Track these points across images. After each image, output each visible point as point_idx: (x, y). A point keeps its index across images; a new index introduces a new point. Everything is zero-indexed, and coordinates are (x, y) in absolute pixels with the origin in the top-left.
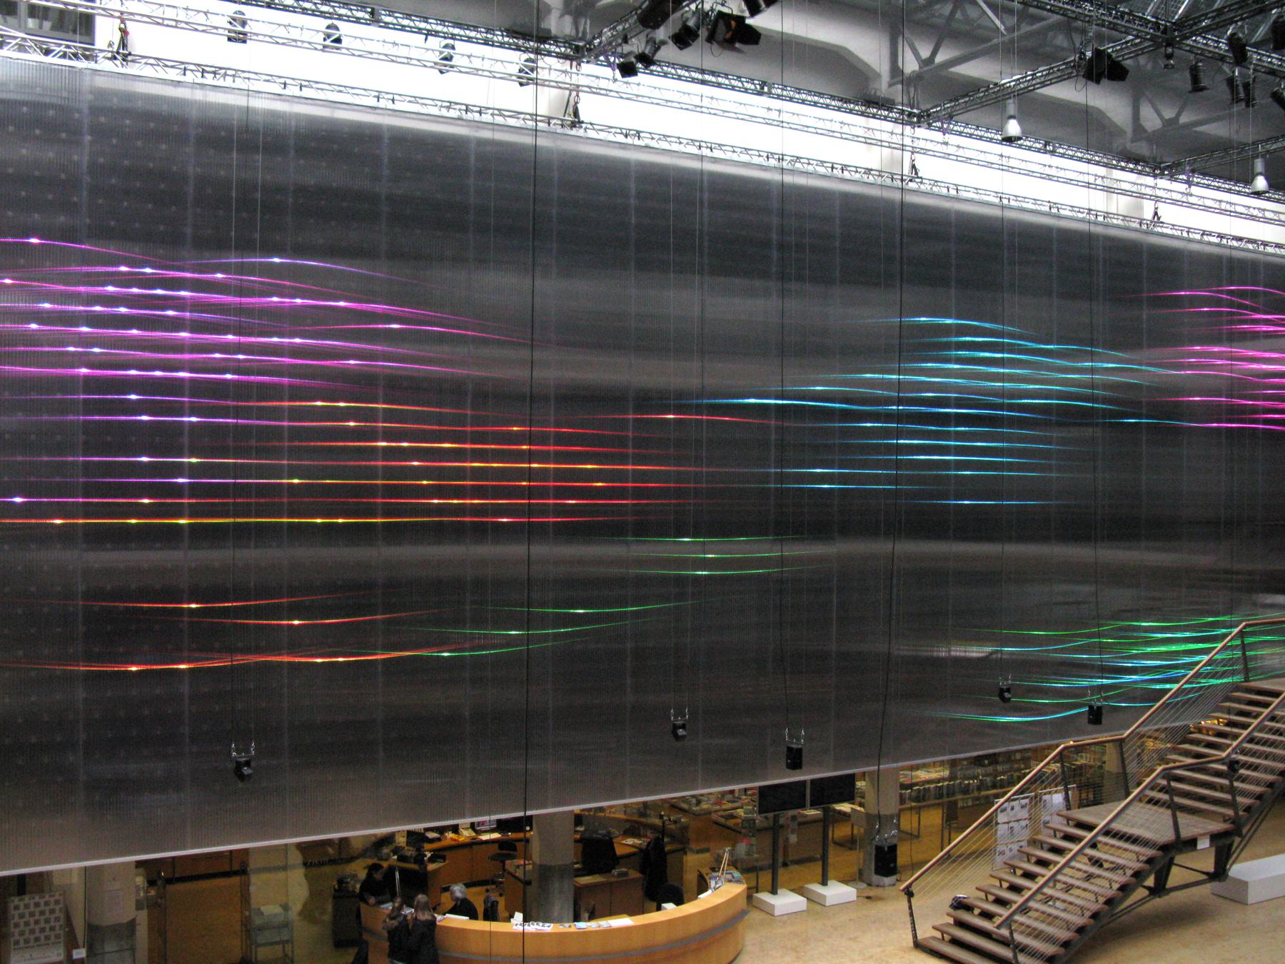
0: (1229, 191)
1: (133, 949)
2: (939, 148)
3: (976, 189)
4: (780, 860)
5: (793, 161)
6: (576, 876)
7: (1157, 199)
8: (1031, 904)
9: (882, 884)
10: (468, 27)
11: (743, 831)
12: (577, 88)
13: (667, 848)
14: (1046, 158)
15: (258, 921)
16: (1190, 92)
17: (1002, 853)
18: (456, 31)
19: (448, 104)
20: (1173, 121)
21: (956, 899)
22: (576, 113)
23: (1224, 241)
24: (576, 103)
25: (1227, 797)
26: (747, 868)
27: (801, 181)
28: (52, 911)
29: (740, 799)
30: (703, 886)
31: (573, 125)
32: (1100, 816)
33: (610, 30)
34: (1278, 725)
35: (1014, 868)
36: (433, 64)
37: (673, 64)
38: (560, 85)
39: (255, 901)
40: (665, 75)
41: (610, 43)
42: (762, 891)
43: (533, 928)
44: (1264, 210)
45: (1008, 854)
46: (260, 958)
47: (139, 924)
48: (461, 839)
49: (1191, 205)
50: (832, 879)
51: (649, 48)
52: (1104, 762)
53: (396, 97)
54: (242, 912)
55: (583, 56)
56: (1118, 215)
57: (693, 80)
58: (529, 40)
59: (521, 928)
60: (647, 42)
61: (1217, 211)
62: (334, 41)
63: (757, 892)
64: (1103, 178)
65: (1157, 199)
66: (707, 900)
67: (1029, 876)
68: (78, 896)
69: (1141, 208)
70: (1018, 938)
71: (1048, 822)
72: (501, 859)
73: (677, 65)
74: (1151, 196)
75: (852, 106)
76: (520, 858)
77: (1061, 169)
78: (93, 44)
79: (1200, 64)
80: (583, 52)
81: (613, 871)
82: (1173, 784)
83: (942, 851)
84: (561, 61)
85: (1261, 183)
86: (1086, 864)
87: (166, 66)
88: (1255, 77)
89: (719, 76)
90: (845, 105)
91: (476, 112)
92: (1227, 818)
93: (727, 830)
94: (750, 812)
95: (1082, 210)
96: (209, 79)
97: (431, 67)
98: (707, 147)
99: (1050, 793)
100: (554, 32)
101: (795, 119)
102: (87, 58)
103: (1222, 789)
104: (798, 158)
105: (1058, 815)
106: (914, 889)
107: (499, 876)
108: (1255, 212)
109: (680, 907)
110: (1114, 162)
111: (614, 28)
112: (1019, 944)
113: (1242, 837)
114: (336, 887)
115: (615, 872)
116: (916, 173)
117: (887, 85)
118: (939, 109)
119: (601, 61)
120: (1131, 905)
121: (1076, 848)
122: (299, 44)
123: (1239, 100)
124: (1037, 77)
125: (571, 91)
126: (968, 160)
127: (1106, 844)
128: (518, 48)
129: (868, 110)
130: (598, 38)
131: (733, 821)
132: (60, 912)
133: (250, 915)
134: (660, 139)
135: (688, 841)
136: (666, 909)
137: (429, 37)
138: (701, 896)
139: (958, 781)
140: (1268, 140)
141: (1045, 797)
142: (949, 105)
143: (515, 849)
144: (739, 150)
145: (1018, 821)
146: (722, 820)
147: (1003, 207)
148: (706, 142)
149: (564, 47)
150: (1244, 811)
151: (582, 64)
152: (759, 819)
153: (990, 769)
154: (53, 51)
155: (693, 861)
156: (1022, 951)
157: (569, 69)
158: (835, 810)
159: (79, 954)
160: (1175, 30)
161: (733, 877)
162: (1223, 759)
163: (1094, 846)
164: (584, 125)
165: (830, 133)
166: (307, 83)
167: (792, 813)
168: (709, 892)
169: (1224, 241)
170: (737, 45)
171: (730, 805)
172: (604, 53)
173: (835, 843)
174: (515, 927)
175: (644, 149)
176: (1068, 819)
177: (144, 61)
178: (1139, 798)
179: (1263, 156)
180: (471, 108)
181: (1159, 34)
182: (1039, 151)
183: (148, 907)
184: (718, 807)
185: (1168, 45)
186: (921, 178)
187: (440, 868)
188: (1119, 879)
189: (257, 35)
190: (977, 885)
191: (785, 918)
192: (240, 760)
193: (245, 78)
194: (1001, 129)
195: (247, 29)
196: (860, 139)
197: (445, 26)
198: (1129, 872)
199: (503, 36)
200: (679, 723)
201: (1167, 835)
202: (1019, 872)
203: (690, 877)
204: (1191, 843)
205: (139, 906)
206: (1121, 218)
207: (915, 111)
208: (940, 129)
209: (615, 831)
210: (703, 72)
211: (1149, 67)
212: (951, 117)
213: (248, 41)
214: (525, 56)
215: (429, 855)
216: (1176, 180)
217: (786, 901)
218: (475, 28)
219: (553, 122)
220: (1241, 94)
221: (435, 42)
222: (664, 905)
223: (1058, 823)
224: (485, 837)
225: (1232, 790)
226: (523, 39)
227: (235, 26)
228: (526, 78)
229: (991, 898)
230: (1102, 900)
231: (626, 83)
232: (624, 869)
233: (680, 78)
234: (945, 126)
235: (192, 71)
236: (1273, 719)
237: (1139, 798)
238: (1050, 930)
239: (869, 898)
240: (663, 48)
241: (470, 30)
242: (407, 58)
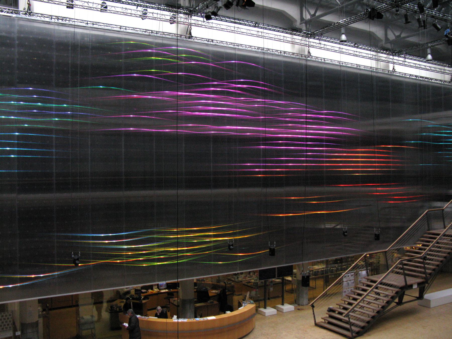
0: (419, 61)
1: (37, 332)
2: (318, 45)
3: (331, 60)
4: (267, 298)
5: (266, 50)
6: (195, 304)
7: (394, 63)
8: (355, 309)
9: (303, 304)
10: (152, 3)
11: (254, 287)
12: (191, 24)
13: (227, 293)
14: (355, 49)
15: (82, 321)
16: (405, 23)
17: (345, 292)
18: (148, 5)
19: (145, 30)
20: (399, 36)
21: (329, 308)
22: (190, 34)
23: (418, 78)
24: (190, 30)
25: (423, 270)
26: (256, 300)
27: (270, 57)
28: (8, 318)
29: (252, 276)
30: (240, 305)
31: (189, 38)
32: (379, 278)
33: (202, 4)
34: (440, 245)
35: (349, 297)
36: (139, 16)
37: (224, 16)
38: (185, 23)
39: (81, 315)
40: (222, 20)
41: (202, 9)
42: (261, 307)
43: (180, 320)
44: (431, 67)
45: (347, 292)
46: (83, 335)
47: (40, 323)
48: (154, 292)
49: (406, 65)
50: (285, 303)
51: (216, 9)
52: (380, 261)
53: (127, 28)
54: (76, 318)
55: (193, 14)
56: (380, 69)
57: (231, 22)
58: (173, 8)
59: (177, 321)
60: (215, 8)
61: (415, 67)
62: (104, 8)
63: (259, 308)
64: (375, 56)
65: (394, 63)
66: (242, 310)
67: (355, 299)
68: (17, 315)
69: (388, 66)
70: (351, 320)
71: (361, 281)
72: (168, 299)
73: (226, 16)
74: (392, 62)
75: (287, 31)
76: (175, 298)
77: (361, 53)
78: (18, 9)
79: (408, 14)
80: (192, 12)
81: (208, 301)
82: (405, 267)
83: (324, 291)
84: (185, 15)
85: (430, 57)
86: (374, 294)
87: (45, 17)
88: (427, 19)
89: (240, 21)
90: (285, 31)
91: (155, 33)
92: (423, 277)
93: (248, 287)
94: (257, 280)
95: (368, 67)
96: (60, 21)
97: (139, 17)
98: (237, 46)
99: (361, 271)
100: (182, 5)
101: (267, 35)
102: (16, 13)
103: (420, 267)
104: (268, 49)
105: (364, 278)
106: (315, 305)
107: (168, 305)
108: (428, 68)
109: (233, 312)
110: (379, 51)
111: (203, 3)
112: (351, 323)
113: (429, 284)
114: (110, 309)
115: (209, 302)
116: (310, 54)
117: (299, 24)
118: (317, 32)
119: (199, 15)
120: (389, 309)
121: (370, 289)
122: (92, 8)
123: (421, 26)
124: (352, 20)
125: (188, 25)
126: (328, 50)
127: (381, 287)
128: (170, 11)
129: (293, 32)
130: (198, 7)
131: (250, 284)
132: (11, 325)
133: (79, 319)
134: (220, 43)
135: (234, 291)
136: (227, 313)
137: (138, 7)
138: (240, 308)
139: (329, 268)
140: (432, 42)
141: (360, 272)
142: (321, 30)
143: (173, 295)
144: (248, 46)
145: (350, 280)
146: (246, 284)
147: (341, 66)
148: (236, 44)
149: (186, 10)
150: (429, 275)
151: (192, 17)
152: (259, 282)
153: (340, 265)
154: (4, 11)
155: (236, 298)
156: (352, 325)
157: (188, 18)
158: (286, 280)
159: (18, 333)
160: (399, 2)
161: (251, 302)
162: (421, 257)
163: (377, 288)
164: (193, 38)
165: (280, 40)
166: (95, 23)
167: (271, 280)
168: (242, 307)
169: (418, 78)
170: (247, 7)
171: (249, 279)
172: (200, 12)
173: (286, 291)
174: (174, 320)
175: (214, 46)
176: (368, 280)
177: (36, 15)
178: (392, 271)
179: (430, 48)
180: (153, 32)
181: (394, 3)
182: (352, 47)
183: (43, 317)
184: (244, 279)
185: (397, 7)
186: (312, 56)
187: (147, 302)
188: (386, 299)
189: (77, 5)
190: (336, 303)
191: (269, 317)
192: (75, 258)
193: (73, 21)
194: (339, 39)
195: (74, 3)
196: (290, 42)
197: (144, 3)
198: (390, 297)
199: (164, 6)
200: (231, 244)
201: (402, 284)
202: (351, 298)
203: (235, 304)
204: (411, 286)
205: (39, 317)
206: (382, 70)
207: (309, 33)
208: (318, 39)
209: (209, 288)
210: (235, 19)
211: (390, 18)
212: (321, 34)
213: (74, 8)
214: (172, 14)
215: (143, 297)
216: (400, 57)
217: (269, 311)
218: (154, 4)
219: (182, 37)
220: (423, 24)
221: (139, 8)
222: (227, 312)
223: (364, 281)
224: (162, 291)
225: (424, 268)
226: (171, 8)
227: (69, 2)
228: (172, 22)
229: (342, 307)
230: (380, 306)
231: (208, 22)
232: (212, 301)
233: (226, 21)
234: (320, 38)
235: (54, 19)
236: (438, 243)
237: (392, 271)
238: (362, 317)
239: (299, 309)
240: (221, 9)
241: (153, 4)
242: (131, 14)
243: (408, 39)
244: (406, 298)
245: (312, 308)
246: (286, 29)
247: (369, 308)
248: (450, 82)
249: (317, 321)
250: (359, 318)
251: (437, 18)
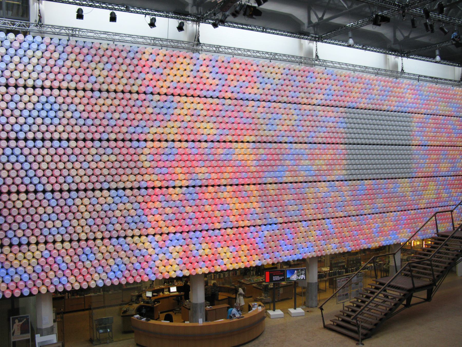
18: (156, 13)
20: (408, 37)
22: (198, 40)
24: (198, 37)
55: (200, 20)
78: (29, 21)
85: (438, 58)
100: (190, 12)
106: (323, 307)
163: (385, 290)
170: (254, 16)
210: (242, 24)
218: (163, 12)
220: (429, 28)
239: (308, 311)
243: (417, 39)
244: (414, 300)
245: (320, 310)
246: (293, 33)
247: (377, 310)
248: (459, 82)
249: (326, 323)
250: (367, 320)
251: (443, 22)
